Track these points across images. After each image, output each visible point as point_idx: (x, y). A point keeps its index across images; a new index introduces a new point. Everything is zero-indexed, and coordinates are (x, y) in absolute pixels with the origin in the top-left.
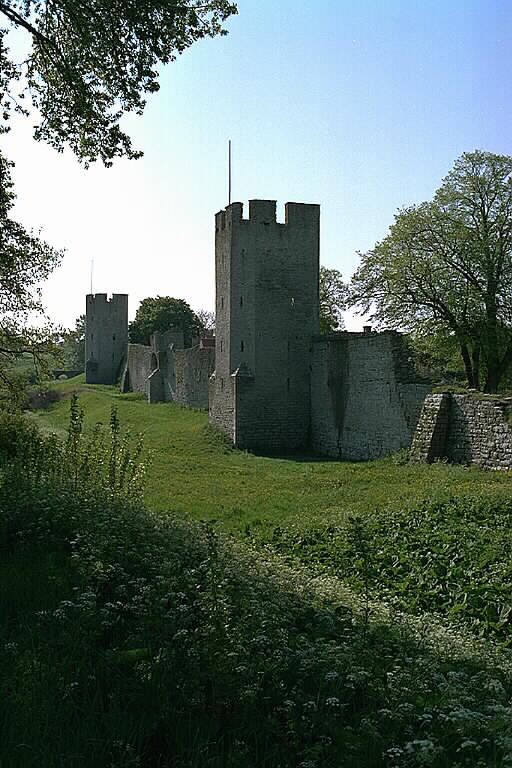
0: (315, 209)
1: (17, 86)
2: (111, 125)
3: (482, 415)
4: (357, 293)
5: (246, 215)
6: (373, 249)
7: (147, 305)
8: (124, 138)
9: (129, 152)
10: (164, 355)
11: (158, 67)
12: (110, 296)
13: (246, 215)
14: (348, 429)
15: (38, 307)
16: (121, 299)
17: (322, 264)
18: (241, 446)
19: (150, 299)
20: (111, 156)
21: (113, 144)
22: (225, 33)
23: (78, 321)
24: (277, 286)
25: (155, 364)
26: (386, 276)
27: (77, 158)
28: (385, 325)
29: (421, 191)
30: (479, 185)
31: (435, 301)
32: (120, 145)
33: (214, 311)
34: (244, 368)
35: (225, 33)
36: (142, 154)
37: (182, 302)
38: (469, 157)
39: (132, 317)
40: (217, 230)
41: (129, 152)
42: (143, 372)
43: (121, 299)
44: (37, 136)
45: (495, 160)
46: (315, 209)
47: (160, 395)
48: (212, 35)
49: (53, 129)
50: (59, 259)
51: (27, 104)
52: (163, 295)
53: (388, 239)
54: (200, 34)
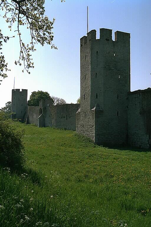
0: (128, 35)
5: (98, 37)
7: (34, 94)
10: (45, 108)
12: (21, 90)
13: (98, 37)
16: (25, 91)
17: (75, 102)
18: (99, 144)
19: (35, 92)
23: (6, 104)
24: (113, 68)
25: (41, 112)
34: (98, 106)
36: (28, 45)
37: (47, 93)
39: (28, 99)
40: (81, 45)
42: (35, 116)
43: (25, 91)
46: (128, 35)
47: (43, 124)
52: (40, 90)
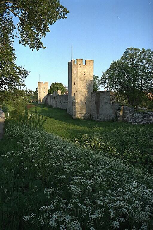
1: (15, 30)
2: (39, 40)
3: (131, 111)
4: (102, 82)
6: (106, 71)
8: (42, 43)
9: (43, 47)
11: (49, 26)
14: (100, 114)
15: (23, 85)
20: (39, 48)
21: (38, 45)
22: (66, 18)
26: (109, 77)
27: (30, 48)
28: (109, 89)
29: (117, 57)
30: (131, 55)
31: (121, 84)
32: (41, 45)
33: (68, 86)
35: (66, 18)
38: (129, 49)
40: (69, 66)
41: (43, 47)
44: (20, 42)
45: (135, 49)
48: (63, 18)
49: (24, 41)
50: (29, 73)
51: (18, 35)
53: (110, 69)
54: (59, 18)
